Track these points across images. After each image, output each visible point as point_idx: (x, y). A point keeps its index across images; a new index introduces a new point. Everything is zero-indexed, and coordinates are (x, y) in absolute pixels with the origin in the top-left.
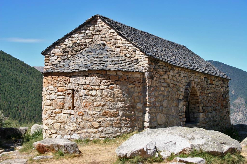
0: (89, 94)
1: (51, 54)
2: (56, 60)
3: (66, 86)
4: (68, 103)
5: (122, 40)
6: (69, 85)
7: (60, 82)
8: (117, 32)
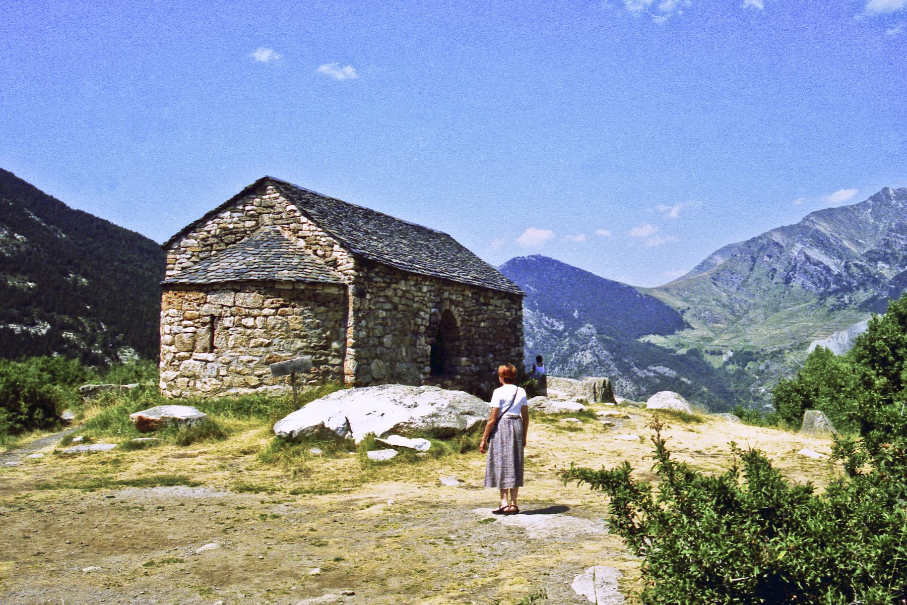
2: (189, 259)
8: (300, 209)
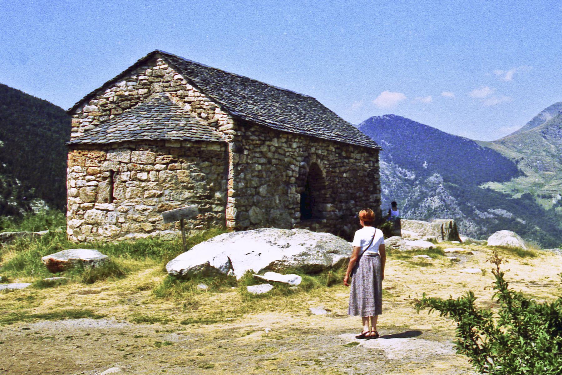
0: (136, 178)
1: (83, 114)
3: (100, 166)
4: (104, 192)
5: (195, 91)
6: (104, 164)
7: (91, 160)
